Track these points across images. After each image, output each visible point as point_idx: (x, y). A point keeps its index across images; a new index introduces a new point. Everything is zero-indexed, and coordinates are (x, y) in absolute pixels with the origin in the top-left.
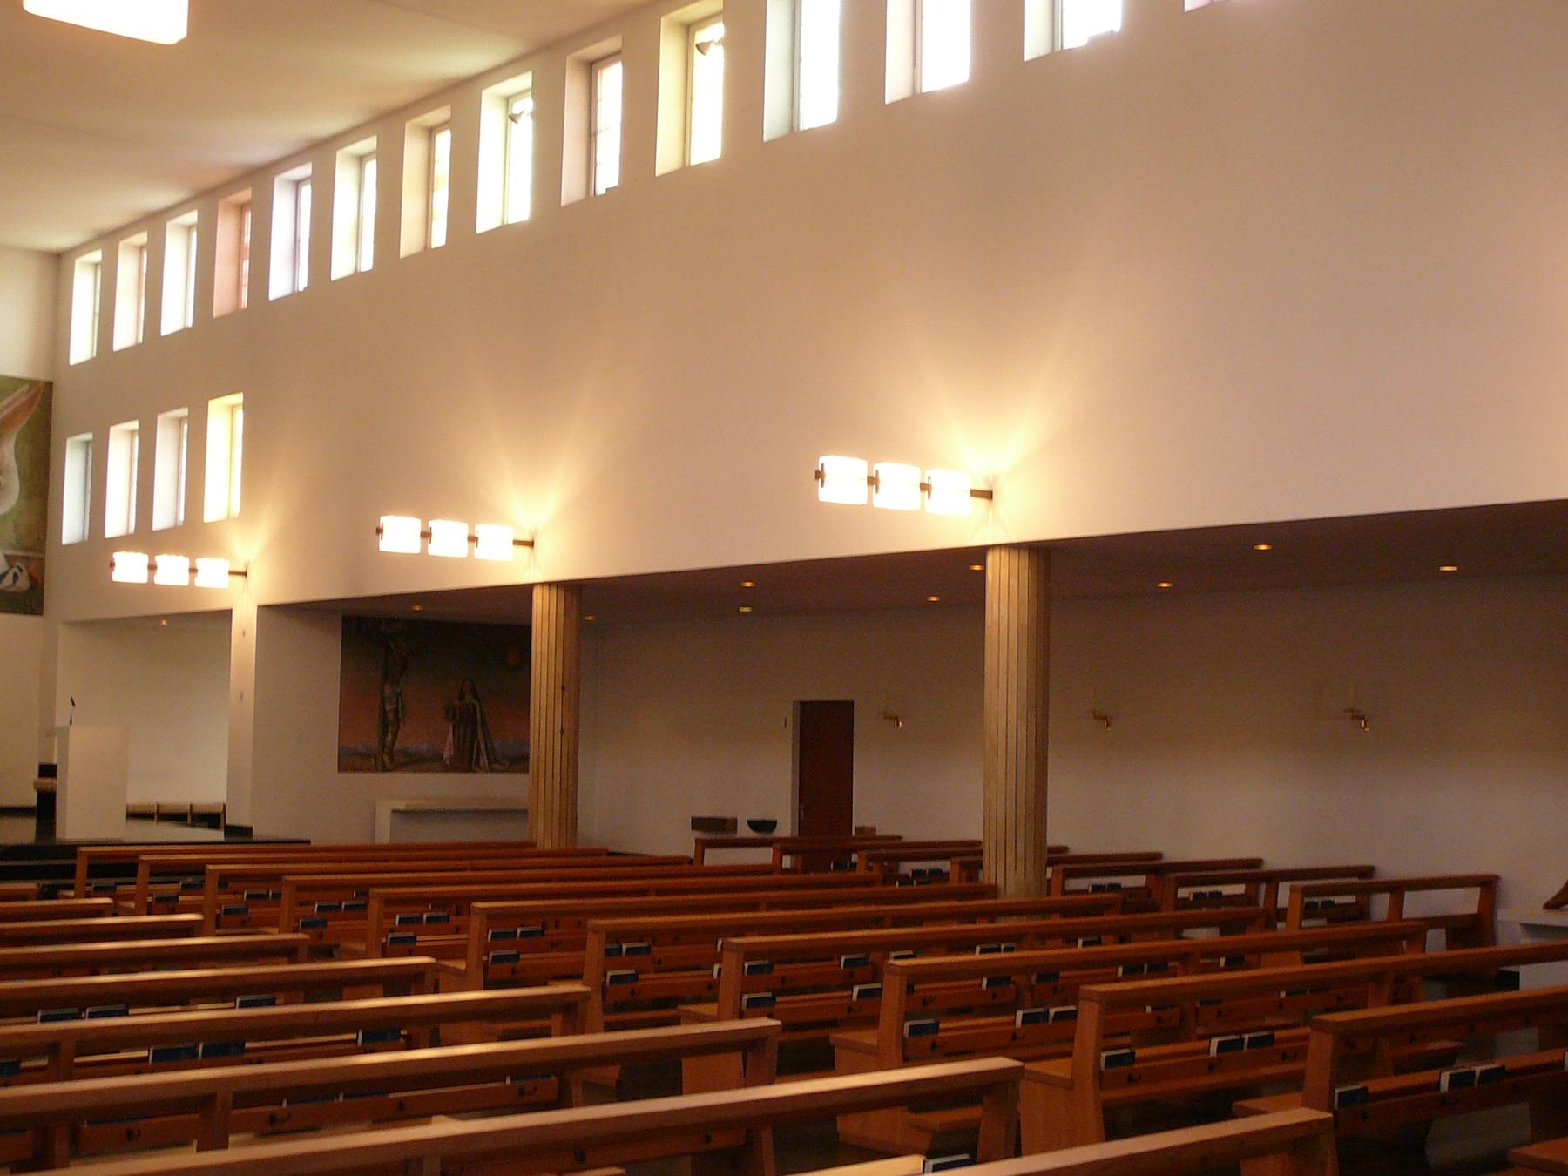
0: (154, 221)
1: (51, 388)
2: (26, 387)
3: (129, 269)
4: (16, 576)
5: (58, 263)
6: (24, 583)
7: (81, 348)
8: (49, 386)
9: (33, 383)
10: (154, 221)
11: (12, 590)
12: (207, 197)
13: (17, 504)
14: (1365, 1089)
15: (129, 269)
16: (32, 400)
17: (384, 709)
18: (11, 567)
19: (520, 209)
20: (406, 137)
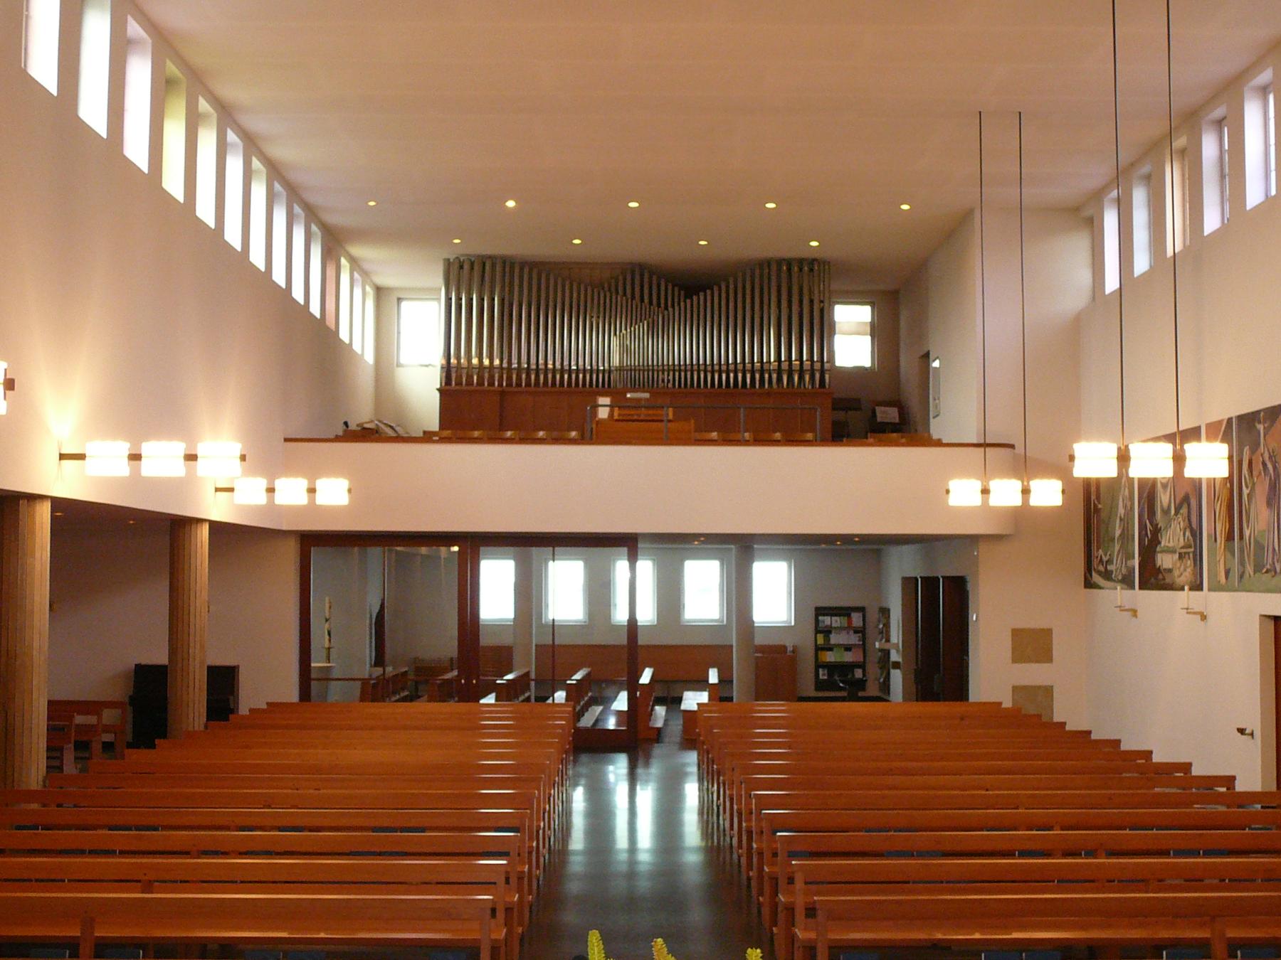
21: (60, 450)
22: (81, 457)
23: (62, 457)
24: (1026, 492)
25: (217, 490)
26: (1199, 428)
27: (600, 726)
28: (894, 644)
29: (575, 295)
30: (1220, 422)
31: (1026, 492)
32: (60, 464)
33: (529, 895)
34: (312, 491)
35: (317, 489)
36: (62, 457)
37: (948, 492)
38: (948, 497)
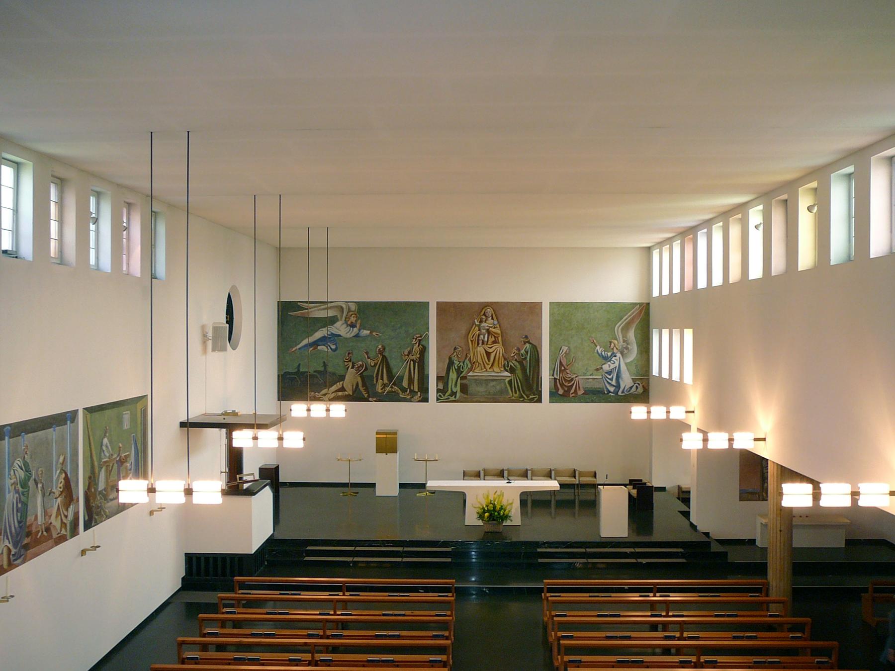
0: (742, 208)
1: (649, 305)
2: (638, 306)
3: (735, 232)
4: (637, 387)
5: (649, 250)
6: (640, 390)
7: (656, 293)
8: (648, 304)
9: (641, 304)
10: (742, 208)
11: (636, 393)
12: (766, 195)
13: (636, 356)
14: (725, 554)
15: (735, 232)
16: (641, 311)
17: (763, 471)
18: (635, 384)
19: (678, 291)
20: (871, 168)
21: (766, 443)
22: (756, 440)
23: (764, 439)
24: (649, 412)
25: (693, 412)
26: (75, 412)
27: (272, 538)
28: (656, 595)
29: (628, 550)
30: (83, 411)
31: (649, 412)
32: (766, 435)
33: (559, 655)
34: (668, 412)
35: (646, 413)
36: (764, 439)
37: (631, 412)
38: (682, 444)
